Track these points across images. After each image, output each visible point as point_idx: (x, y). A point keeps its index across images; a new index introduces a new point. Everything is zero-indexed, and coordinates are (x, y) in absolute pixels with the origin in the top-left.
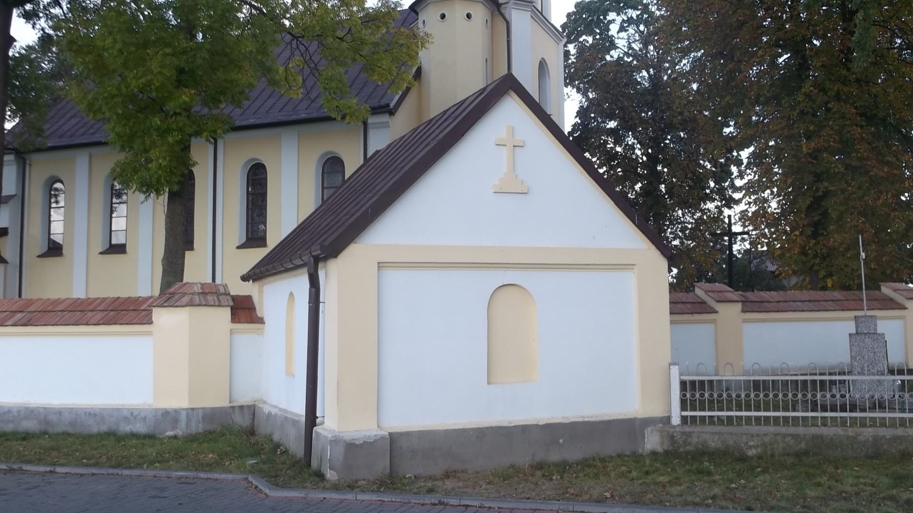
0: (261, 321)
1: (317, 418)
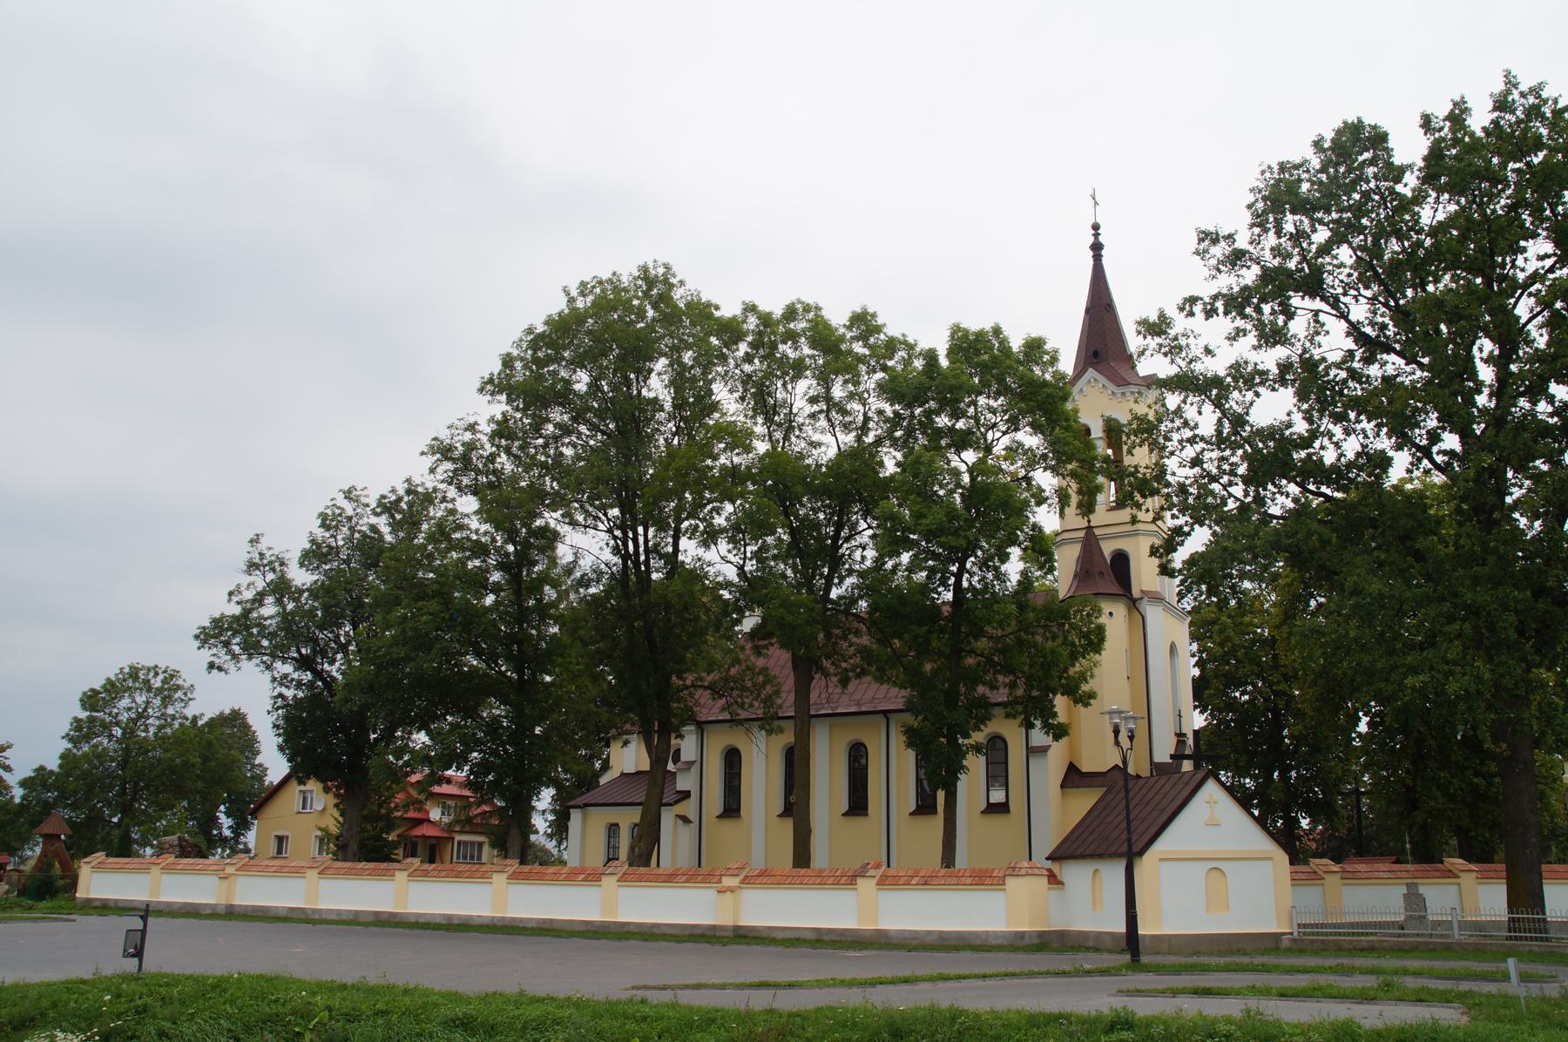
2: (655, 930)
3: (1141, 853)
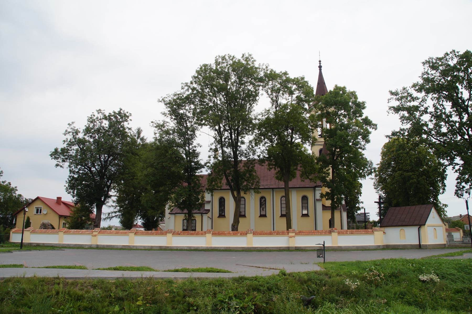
2: (267, 249)
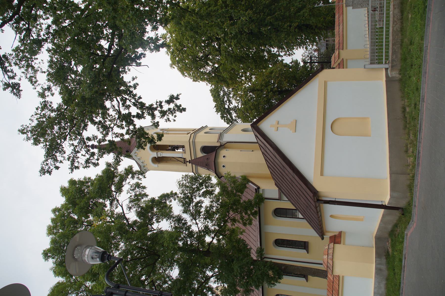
0: (340, 233)
1: (382, 204)
3: (315, 192)
